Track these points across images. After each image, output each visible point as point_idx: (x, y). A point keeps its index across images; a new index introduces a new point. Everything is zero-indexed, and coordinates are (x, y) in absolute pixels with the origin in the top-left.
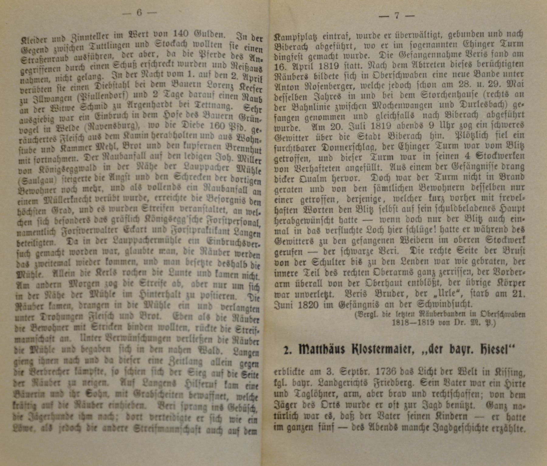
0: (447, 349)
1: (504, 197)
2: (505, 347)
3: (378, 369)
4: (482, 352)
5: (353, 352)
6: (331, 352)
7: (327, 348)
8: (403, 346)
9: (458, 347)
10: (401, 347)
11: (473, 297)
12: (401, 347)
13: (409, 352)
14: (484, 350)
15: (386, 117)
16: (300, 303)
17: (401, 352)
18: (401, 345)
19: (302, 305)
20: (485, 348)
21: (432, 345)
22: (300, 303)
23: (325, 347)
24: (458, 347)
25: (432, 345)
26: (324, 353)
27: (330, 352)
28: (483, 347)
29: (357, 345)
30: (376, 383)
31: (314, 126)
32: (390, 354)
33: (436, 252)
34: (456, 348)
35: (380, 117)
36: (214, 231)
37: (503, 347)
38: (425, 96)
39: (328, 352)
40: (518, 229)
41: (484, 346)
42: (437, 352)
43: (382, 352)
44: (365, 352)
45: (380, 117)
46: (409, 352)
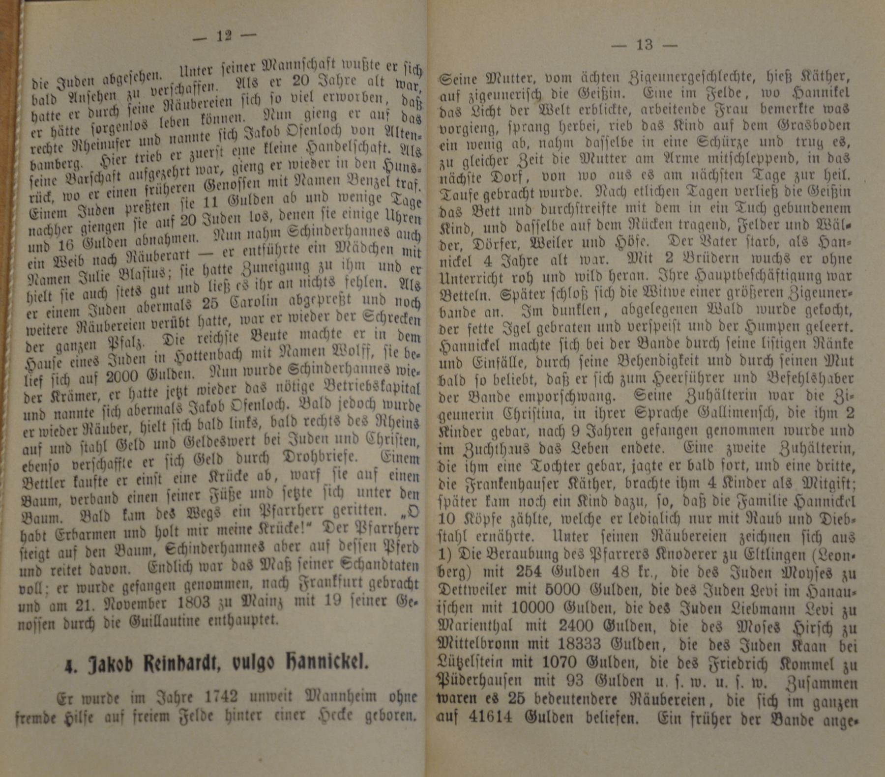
0: (139, 663)
1: (698, 717)
2: (358, 657)
3: (208, 693)
4: (288, 666)
5: (146, 669)
6: (191, 668)
7: (183, 660)
8: (333, 657)
9: (191, 659)
10: (330, 658)
11: (84, 453)
12: (330, 658)
13: (361, 667)
14: (292, 663)
15: (480, 163)
16: (562, 640)
17: (330, 667)
18: (330, 654)
19: (565, 643)
20: (294, 659)
21: (208, 655)
22: (562, 640)
23: (181, 660)
24: (191, 659)
25: (208, 655)
26: (179, 669)
27: (188, 668)
28: (290, 658)
29: (349, 657)
30: (183, 716)
31: (240, 81)
32: (312, 670)
33: (315, 423)
34: (187, 661)
35: (470, 164)
36: (576, 310)
37: (355, 658)
38: (641, 398)
39: (186, 669)
40: (660, 607)
41: (291, 655)
42: (355, 667)
43: (164, 669)
44: (120, 670)
45: (470, 164)
46: (361, 667)
